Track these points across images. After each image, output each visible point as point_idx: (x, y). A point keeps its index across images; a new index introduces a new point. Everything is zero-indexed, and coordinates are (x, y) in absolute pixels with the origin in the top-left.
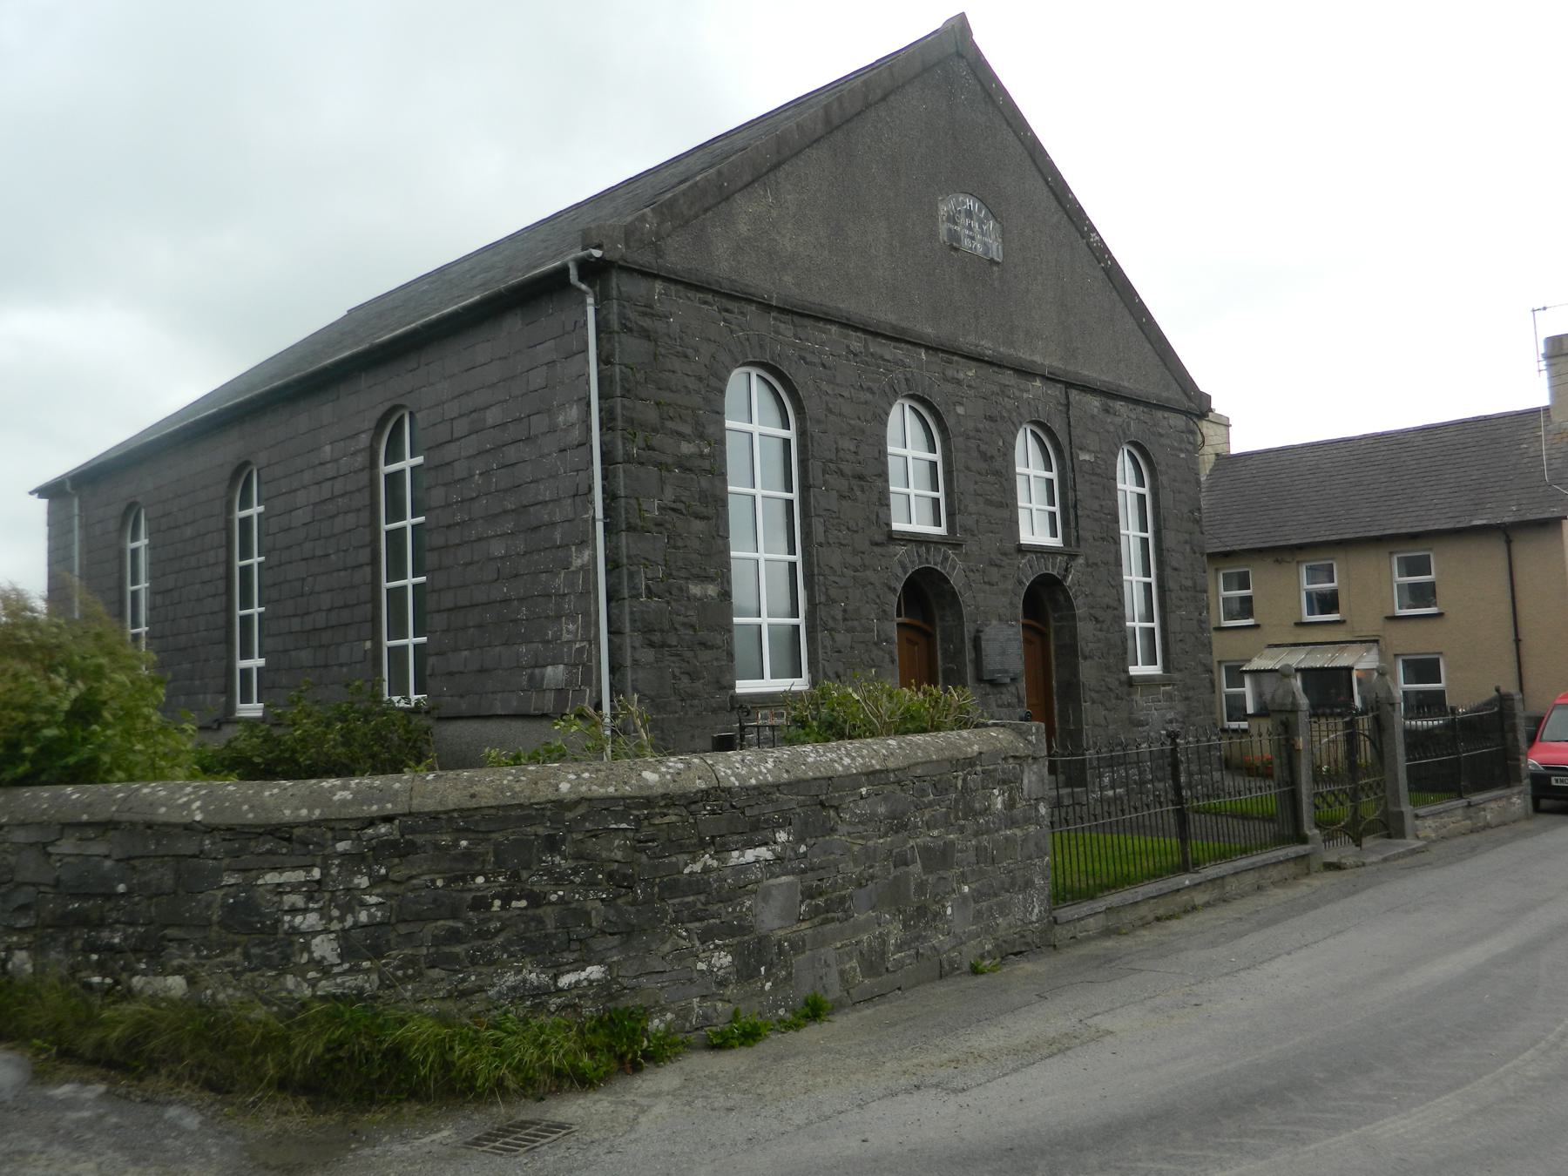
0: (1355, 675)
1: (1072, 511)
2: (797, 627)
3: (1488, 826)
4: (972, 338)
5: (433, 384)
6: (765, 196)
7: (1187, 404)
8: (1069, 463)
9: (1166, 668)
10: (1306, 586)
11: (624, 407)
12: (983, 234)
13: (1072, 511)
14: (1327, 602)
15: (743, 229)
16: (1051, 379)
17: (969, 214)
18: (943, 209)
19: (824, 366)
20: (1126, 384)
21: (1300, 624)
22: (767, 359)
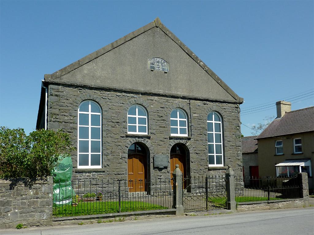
0: (300, 167)
1: (190, 128)
2: (222, 155)
3: (280, 208)
4: (157, 90)
5: (301, 111)
6: (93, 65)
7: (234, 101)
8: (189, 117)
9: (224, 165)
10: (295, 145)
11: (50, 110)
12: (162, 66)
13: (190, 128)
14: (299, 149)
15: (86, 72)
16: (184, 98)
17: (158, 62)
18: (149, 62)
19: (108, 99)
20: (212, 97)
21: (293, 154)
22: (92, 98)
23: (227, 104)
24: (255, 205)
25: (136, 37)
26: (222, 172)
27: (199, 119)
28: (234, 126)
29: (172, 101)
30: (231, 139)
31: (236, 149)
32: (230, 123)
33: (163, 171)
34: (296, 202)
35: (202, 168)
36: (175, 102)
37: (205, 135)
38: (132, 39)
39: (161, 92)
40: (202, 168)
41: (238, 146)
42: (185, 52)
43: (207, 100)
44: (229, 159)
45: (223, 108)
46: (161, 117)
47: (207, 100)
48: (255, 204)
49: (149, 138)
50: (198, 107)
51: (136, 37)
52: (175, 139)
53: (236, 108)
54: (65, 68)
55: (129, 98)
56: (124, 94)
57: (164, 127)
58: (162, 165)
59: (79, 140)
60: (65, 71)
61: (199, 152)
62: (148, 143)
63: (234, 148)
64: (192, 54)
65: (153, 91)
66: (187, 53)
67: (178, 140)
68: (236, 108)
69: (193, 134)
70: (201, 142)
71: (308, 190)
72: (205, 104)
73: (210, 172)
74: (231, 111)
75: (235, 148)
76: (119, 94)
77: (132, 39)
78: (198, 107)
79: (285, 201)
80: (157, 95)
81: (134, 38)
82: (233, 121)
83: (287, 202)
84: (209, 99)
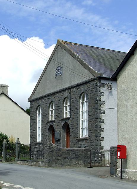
44: (90, 130)
50: (74, 93)
57: (60, 113)
62: (54, 125)
78: (74, 93)
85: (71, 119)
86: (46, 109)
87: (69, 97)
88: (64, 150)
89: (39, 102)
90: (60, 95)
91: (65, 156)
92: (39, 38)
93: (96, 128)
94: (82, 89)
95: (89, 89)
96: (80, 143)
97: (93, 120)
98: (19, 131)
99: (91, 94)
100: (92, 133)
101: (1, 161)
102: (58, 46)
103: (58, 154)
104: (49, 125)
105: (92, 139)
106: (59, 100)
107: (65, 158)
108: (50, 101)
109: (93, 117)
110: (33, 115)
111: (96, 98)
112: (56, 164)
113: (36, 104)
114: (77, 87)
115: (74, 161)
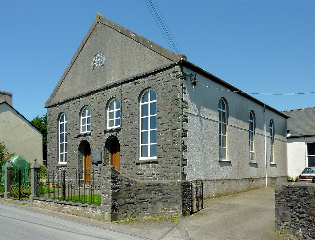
23: (161, 72)
24: (47, 203)
25: (85, 44)
26: (152, 167)
27: (129, 104)
28: (171, 101)
29: (107, 93)
30: (165, 121)
31: (172, 134)
32: (165, 98)
33: (99, 165)
34: (89, 209)
35: (130, 162)
36: (109, 93)
37: (135, 122)
38: (82, 48)
39: (98, 87)
40: (130, 162)
41: (174, 129)
42: (118, 31)
43: (137, 78)
44: (162, 148)
45: (156, 80)
46: (98, 112)
47: (137, 78)
48: (47, 201)
49: (89, 135)
50: (129, 91)
51: (85, 44)
52: (108, 133)
53: (174, 72)
54: (52, 95)
55: (80, 102)
56: (77, 100)
57: (100, 122)
58: (96, 160)
59: (150, 143)
60: (53, 96)
61: (128, 143)
62: (89, 139)
63: (169, 133)
64: (123, 30)
65: (93, 89)
66: (120, 32)
67: (110, 133)
68: (174, 72)
69: (123, 124)
70: (130, 131)
71: (109, 195)
72: (135, 84)
73: (138, 166)
74: (166, 80)
75: (171, 132)
76: (74, 101)
77: (82, 48)
78: (129, 91)
79: (74, 205)
80: (95, 92)
81: (84, 46)
82: (169, 94)
83: (77, 207)
84: (138, 75)
85: (122, 130)
86: (75, 117)
87: (117, 96)
88: (141, 185)
89: (62, 107)
90: (101, 95)
91: (143, 196)
92: (4, 150)
93: (175, 143)
94: (144, 83)
95: (159, 82)
96: (140, 167)
97: (168, 131)
98: (25, 147)
99: (164, 90)
100: (165, 153)
101: (2, 196)
102: (98, 23)
103: (129, 192)
104: (81, 139)
105: (165, 162)
106: (99, 103)
107: (143, 200)
108: (82, 105)
109: (168, 127)
110: (53, 127)
111: (176, 96)
112: (125, 214)
113: (56, 111)
114: (135, 81)
115: (160, 205)
